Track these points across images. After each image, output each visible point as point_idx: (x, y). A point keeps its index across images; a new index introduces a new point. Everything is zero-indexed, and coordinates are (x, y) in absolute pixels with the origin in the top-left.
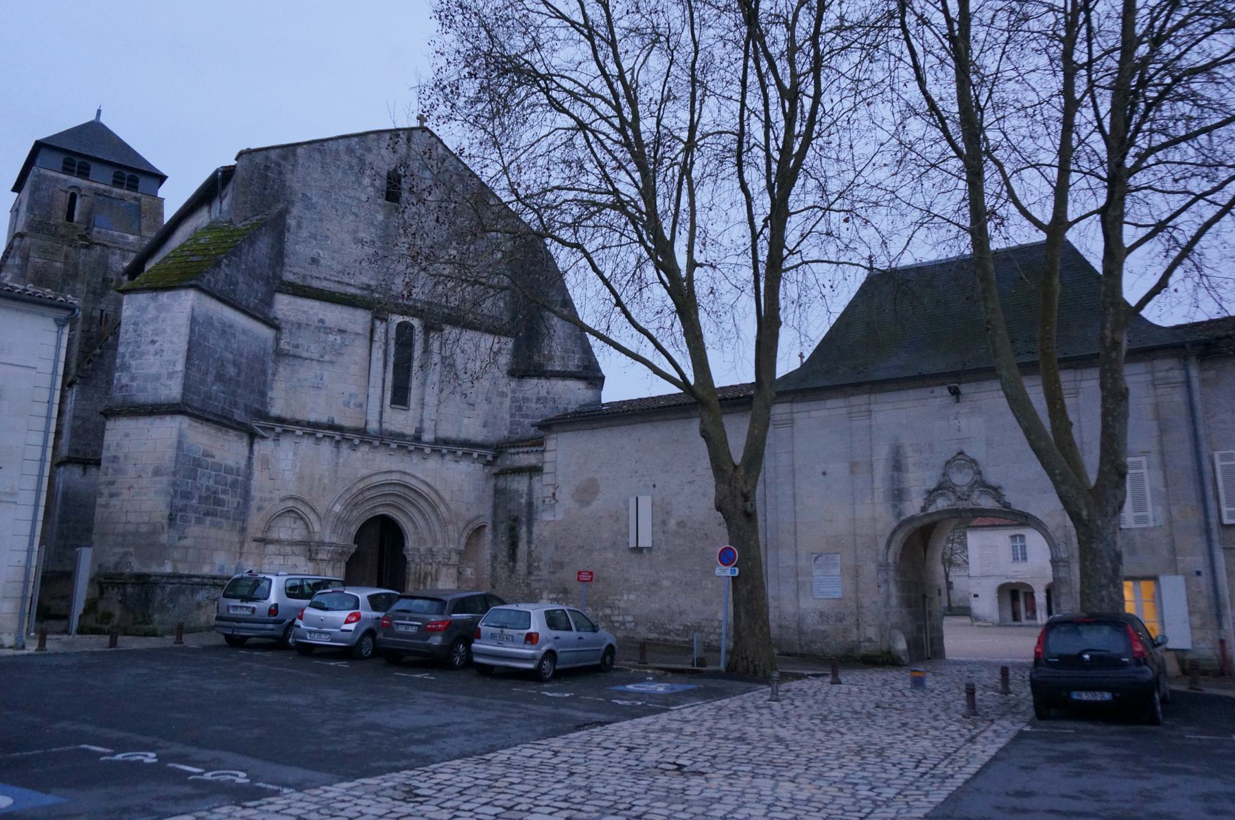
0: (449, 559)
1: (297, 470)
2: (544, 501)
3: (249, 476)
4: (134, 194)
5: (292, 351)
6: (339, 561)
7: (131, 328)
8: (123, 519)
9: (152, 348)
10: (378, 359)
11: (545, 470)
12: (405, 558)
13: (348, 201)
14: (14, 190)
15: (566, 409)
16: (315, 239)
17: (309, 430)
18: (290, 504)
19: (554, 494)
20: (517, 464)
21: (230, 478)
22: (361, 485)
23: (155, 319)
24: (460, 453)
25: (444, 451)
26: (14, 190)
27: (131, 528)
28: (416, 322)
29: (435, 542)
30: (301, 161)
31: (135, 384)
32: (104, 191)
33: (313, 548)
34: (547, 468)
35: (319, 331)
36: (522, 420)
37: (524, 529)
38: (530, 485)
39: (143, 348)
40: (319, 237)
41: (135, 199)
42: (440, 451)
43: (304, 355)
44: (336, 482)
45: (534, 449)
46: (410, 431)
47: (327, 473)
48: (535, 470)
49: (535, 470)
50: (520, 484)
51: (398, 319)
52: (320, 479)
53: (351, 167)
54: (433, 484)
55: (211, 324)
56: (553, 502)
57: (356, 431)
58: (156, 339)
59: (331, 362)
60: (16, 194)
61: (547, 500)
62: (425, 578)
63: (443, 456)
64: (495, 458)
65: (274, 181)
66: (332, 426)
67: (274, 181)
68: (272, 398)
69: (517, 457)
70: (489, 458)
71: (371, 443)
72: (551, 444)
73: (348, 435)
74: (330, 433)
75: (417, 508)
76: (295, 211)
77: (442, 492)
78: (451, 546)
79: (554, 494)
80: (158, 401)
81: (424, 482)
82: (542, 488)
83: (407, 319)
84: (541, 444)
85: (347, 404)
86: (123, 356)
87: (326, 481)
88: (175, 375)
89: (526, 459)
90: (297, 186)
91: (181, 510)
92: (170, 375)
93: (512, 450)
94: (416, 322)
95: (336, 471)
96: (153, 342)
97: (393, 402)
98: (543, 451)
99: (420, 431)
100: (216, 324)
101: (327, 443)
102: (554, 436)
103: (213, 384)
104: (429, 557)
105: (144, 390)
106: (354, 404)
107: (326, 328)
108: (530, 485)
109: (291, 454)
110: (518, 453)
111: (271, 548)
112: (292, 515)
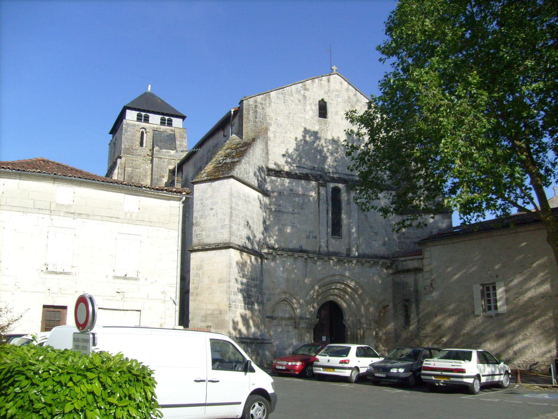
0: (370, 325)
2: (425, 289)
3: (262, 281)
4: (171, 128)
6: (310, 328)
7: (199, 202)
8: (205, 307)
9: (212, 213)
10: (323, 210)
11: (424, 270)
12: (344, 325)
13: (299, 120)
14: (111, 133)
15: (431, 232)
16: (284, 143)
17: (290, 253)
19: (431, 284)
20: (406, 268)
23: (212, 196)
24: (372, 262)
25: (364, 261)
26: (111, 133)
27: (209, 312)
28: (341, 186)
30: (273, 101)
31: (204, 233)
32: (157, 128)
33: (297, 321)
34: (426, 269)
35: (291, 196)
36: (405, 240)
37: (414, 306)
38: (416, 279)
39: (206, 213)
40: (285, 142)
41: (172, 130)
42: (361, 262)
43: (284, 210)
45: (416, 257)
46: (343, 250)
48: (418, 270)
49: (418, 270)
50: (409, 279)
51: (332, 185)
53: (300, 101)
55: (239, 197)
56: (431, 289)
57: (314, 253)
58: (213, 207)
59: (298, 213)
60: (111, 135)
61: (427, 288)
63: (363, 264)
64: (392, 264)
65: (260, 113)
66: (301, 251)
67: (260, 113)
69: (405, 263)
70: (388, 264)
71: (323, 259)
72: (427, 254)
73: (311, 255)
74: (300, 254)
76: (272, 129)
78: (371, 318)
79: (431, 284)
80: (218, 242)
82: (423, 280)
83: (337, 185)
84: (421, 254)
85: (308, 237)
86: (196, 218)
88: (226, 226)
89: (412, 264)
90: (272, 115)
91: (234, 302)
92: (223, 227)
93: (402, 259)
94: (341, 186)
96: (212, 209)
97: (333, 234)
98: (422, 259)
99: (349, 250)
100: (242, 196)
102: (428, 249)
103: (243, 230)
104: (358, 324)
105: (208, 236)
106: (312, 237)
107: (294, 194)
108: (416, 279)
110: (406, 260)
111: (275, 322)
112: (285, 302)
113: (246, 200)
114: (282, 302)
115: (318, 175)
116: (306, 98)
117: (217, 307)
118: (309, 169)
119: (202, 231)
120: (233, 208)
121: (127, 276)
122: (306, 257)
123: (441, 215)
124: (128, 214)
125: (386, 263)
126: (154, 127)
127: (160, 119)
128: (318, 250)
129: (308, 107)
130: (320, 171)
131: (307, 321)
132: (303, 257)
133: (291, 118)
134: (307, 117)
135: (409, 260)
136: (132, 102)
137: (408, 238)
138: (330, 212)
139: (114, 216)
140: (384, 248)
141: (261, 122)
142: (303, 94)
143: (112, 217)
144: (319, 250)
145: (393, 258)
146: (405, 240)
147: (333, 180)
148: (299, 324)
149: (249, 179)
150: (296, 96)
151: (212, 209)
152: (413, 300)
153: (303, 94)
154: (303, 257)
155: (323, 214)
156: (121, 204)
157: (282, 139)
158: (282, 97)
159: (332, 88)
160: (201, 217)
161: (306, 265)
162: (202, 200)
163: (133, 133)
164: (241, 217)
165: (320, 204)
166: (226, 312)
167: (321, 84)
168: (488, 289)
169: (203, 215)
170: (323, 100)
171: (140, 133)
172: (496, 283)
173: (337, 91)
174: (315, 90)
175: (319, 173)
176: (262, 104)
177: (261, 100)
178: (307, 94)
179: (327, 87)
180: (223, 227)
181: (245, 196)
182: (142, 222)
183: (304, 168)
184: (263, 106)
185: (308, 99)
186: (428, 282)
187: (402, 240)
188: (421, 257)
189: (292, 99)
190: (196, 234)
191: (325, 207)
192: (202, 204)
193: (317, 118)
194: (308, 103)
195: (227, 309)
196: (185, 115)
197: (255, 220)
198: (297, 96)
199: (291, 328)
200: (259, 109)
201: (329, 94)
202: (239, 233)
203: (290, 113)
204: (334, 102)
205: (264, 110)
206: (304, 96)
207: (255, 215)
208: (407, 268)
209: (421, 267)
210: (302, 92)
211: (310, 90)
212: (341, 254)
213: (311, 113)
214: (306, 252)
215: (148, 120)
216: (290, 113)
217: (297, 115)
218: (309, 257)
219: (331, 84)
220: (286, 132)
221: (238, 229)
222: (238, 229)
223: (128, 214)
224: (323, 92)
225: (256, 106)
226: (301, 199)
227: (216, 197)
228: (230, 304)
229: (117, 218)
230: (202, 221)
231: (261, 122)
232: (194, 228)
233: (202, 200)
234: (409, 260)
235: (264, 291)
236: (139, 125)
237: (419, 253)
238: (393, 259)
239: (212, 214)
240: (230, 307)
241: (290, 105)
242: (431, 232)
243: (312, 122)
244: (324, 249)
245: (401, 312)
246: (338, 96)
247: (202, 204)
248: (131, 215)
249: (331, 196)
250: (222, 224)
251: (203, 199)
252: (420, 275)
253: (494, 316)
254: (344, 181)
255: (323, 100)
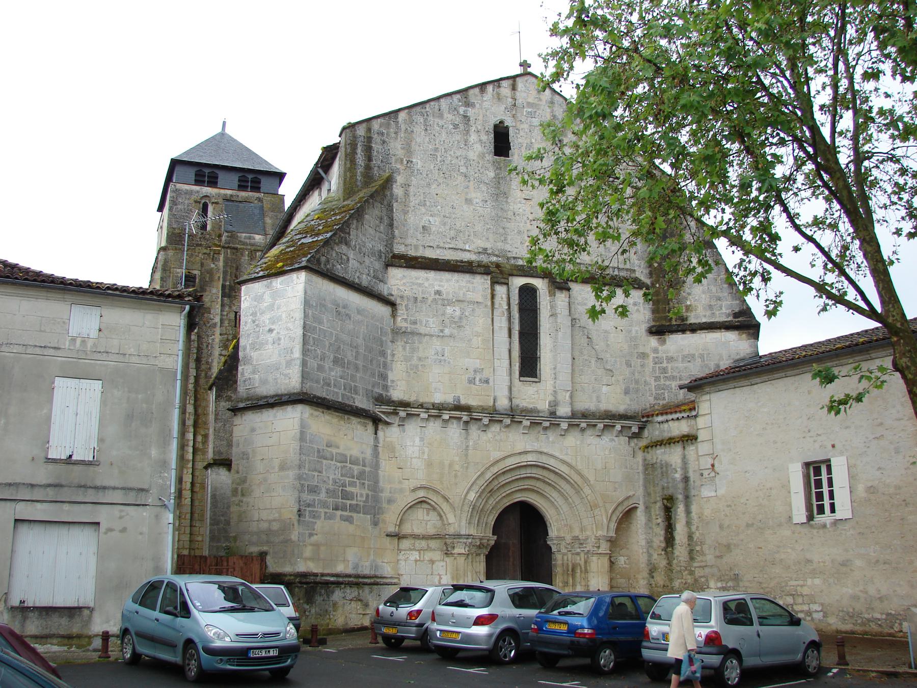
1: (426, 457)
2: (702, 475)
3: (376, 466)
4: (256, 195)
5: (410, 328)
9: (270, 337)
16: (425, 205)
18: (421, 494)
19: (713, 466)
20: (666, 435)
21: (356, 469)
22: (495, 469)
23: (271, 307)
24: (601, 426)
29: (582, 529)
32: (231, 196)
34: (702, 436)
36: (668, 383)
38: (684, 458)
40: (428, 204)
44: (467, 468)
47: (457, 459)
48: (689, 439)
49: (689, 439)
50: (673, 456)
52: (451, 465)
53: (456, 126)
54: (574, 464)
56: (713, 474)
57: (483, 410)
58: (273, 327)
61: (706, 473)
62: (573, 570)
65: (378, 152)
66: (458, 408)
67: (378, 152)
68: (393, 381)
69: (666, 425)
70: (635, 429)
75: (559, 491)
76: (400, 179)
77: (585, 472)
81: (564, 462)
84: (694, 409)
85: (472, 381)
86: (245, 349)
87: (457, 467)
89: (679, 428)
91: (309, 505)
93: (660, 418)
95: (466, 455)
97: (521, 375)
101: (455, 426)
102: (707, 397)
103: (331, 370)
106: (480, 380)
108: (684, 458)
109: (417, 440)
113: (338, 313)
114: (419, 506)
115: (492, 263)
116: (469, 120)
117: (277, 515)
118: (475, 253)
119: (254, 372)
120: (307, 327)
121: (74, 458)
122: (465, 418)
123: (737, 332)
124: (78, 341)
125: (630, 427)
126: (225, 195)
127: (194, 174)
128: (491, 404)
129: (473, 137)
130: (497, 256)
131: (470, 540)
132: (460, 419)
133: (439, 159)
134: (472, 155)
135: (673, 419)
136: (187, 153)
137: (673, 378)
138: (517, 333)
139: (49, 345)
140: (627, 399)
141: (379, 167)
142: (462, 113)
143: (45, 347)
144: (494, 405)
145: (643, 417)
146: (668, 383)
147: (523, 271)
148: (454, 547)
149: (347, 273)
150: (448, 116)
151: (271, 331)
152: (680, 497)
153: (462, 113)
154: (460, 419)
155: (502, 336)
156: (64, 322)
157: (422, 198)
158: (422, 120)
159: (519, 102)
160: (254, 347)
161: (468, 434)
162: (254, 314)
163: (188, 206)
164: (327, 343)
165: (495, 318)
166: (293, 525)
167: (498, 94)
168: (818, 472)
169: (256, 343)
170: (501, 122)
171: (201, 205)
172: (832, 459)
173: (529, 105)
174: (486, 105)
175: (494, 259)
176: (382, 134)
177: (381, 127)
178: (471, 112)
179: (510, 100)
180: (289, 363)
181: (338, 305)
182: (105, 355)
183: (465, 250)
184: (385, 138)
185: (472, 123)
186: (706, 463)
187: (662, 382)
188: (694, 413)
189: (441, 123)
190: (243, 379)
191: (505, 324)
192: (254, 322)
193: (490, 157)
194: (473, 129)
195: (295, 518)
196: (282, 169)
197: (361, 351)
198: (450, 117)
199: (437, 555)
200: (376, 143)
201: (514, 112)
202: (322, 375)
203: (436, 150)
204: (525, 126)
205: (385, 145)
206: (465, 117)
207: (360, 341)
208: (669, 435)
209: (693, 432)
210: (462, 110)
211: (477, 106)
212: (539, 412)
213: (478, 148)
214: (467, 409)
215: (260, 188)
216: (436, 150)
217: (452, 153)
218: (471, 419)
219: (518, 94)
220: (429, 185)
221: (320, 368)
222: (320, 368)
223: (78, 341)
224: (502, 108)
225: (369, 139)
226: (457, 309)
227: (278, 309)
228: (299, 511)
229: (55, 348)
230: (254, 355)
231: (379, 167)
232: (240, 368)
233: (254, 314)
234: (673, 419)
235: (381, 484)
236: (198, 192)
237: (692, 407)
238: (644, 420)
239: (270, 340)
240: (299, 516)
241: (437, 134)
242: (718, 366)
243: (480, 165)
244: (503, 403)
245: (659, 521)
246: (531, 115)
247: (254, 322)
248: (84, 342)
249: (517, 302)
250: (288, 358)
251: (256, 313)
252: (692, 448)
253: (828, 526)
254: (545, 274)
255: (501, 122)
